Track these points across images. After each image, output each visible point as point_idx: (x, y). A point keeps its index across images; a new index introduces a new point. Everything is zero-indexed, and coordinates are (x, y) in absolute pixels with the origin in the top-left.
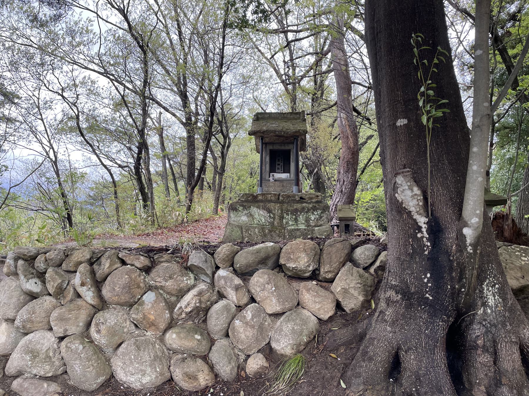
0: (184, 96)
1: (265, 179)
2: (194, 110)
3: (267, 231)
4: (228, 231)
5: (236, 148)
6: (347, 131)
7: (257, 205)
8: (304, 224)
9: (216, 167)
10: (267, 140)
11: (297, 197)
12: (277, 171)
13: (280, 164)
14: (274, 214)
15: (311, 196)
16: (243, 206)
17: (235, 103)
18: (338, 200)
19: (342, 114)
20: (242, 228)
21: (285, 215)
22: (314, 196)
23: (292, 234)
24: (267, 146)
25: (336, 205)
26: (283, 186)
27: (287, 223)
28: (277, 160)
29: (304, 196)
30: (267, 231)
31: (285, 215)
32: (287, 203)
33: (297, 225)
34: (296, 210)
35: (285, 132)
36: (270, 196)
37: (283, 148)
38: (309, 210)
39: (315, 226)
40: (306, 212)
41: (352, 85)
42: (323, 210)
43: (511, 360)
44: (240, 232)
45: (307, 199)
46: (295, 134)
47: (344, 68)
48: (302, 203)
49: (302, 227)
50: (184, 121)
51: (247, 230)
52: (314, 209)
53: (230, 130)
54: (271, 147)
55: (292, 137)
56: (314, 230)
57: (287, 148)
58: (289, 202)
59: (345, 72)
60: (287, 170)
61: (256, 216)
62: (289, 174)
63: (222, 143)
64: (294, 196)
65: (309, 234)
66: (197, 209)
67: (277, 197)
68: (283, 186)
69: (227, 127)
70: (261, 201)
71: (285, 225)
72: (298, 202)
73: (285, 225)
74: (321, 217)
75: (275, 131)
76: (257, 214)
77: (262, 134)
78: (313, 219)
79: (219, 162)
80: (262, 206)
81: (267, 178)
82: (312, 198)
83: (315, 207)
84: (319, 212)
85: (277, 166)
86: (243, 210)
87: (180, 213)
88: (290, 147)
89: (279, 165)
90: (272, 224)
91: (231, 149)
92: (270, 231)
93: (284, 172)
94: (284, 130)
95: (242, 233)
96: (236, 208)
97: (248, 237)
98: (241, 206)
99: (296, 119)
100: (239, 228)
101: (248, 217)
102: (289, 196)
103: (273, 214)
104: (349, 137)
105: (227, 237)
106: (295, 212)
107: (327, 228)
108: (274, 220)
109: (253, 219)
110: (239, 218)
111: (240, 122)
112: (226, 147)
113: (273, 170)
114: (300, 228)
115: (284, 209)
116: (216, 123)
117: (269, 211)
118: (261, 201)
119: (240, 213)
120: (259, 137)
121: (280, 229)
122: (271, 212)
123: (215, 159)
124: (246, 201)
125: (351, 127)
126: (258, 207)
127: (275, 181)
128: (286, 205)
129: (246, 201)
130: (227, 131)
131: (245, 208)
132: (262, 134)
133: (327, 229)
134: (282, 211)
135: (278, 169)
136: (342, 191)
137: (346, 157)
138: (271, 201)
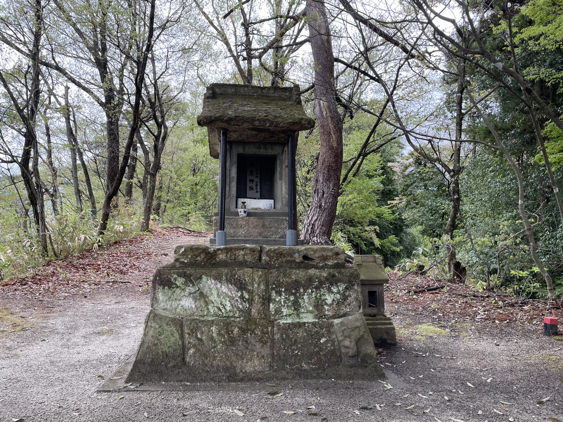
0: (102, 65)
1: (229, 209)
2: (118, 87)
3: (236, 330)
4: (151, 333)
5: (175, 140)
6: (328, 124)
7: (214, 272)
8: (311, 312)
9: (147, 164)
10: (233, 136)
11: (297, 255)
12: (249, 193)
13: (254, 181)
14: (250, 292)
15: (325, 254)
16: (184, 275)
17: (173, 84)
18: (315, 218)
19: (321, 102)
20: (181, 326)
21: (274, 294)
22: (330, 254)
23: (288, 336)
24: (234, 147)
25: (313, 225)
26: (264, 226)
27: (278, 311)
29: (310, 254)
30: (236, 330)
31: (274, 294)
32: (278, 268)
33: (298, 315)
34: (297, 284)
35: (271, 123)
36: (242, 252)
37: (263, 152)
38: (321, 283)
39: (334, 317)
40: (317, 288)
41: (335, 63)
42: (350, 282)
44: (177, 335)
45: (317, 261)
46: (291, 128)
47: (325, 38)
48: (307, 267)
49: (308, 318)
50: (104, 101)
51: (193, 332)
52: (332, 280)
53: (166, 117)
54: (241, 150)
55: (283, 132)
56: (332, 325)
57: (270, 152)
58: (280, 266)
59: (326, 44)
60: (267, 192)
61: (213, 297)
62: (272, 201)
63: (156, 134)
64: (291, 253)
65: (323, 336)
66: (116, 226)
67: (257, 255)
68: (264, 226)
69: (162, 112)
70: (225, 264)
71: (275, 315)
72: (299, 266)
73: (275, 315)
74: (345, 298)
75: (252, 120)
76: (215, 292)
77: (224, 125)
78: (329, 301)
79: (152, 159)
80: (226, 275)
82: (325, 258)
83: (334, 276)
84: (342, 287)
85: (249, 184)
86: (186, 284)
87: (89, 233)
88: (276, 150)
89: (252, 181)
90: (247, 313)
91: (168, 142)
92: (243, 331)
93: (262, 197)
94: (270, 117)
95: (182, 337)
96: (169, 280)
97: (194, 346)
98: (180, 276)
99: (284, 100)
100: (175, 325)
101: (195, 299)
102: (280, 254)
103: (249, 292)
104: (332, 133)
105: (149, 347)
106: (294, 288)
107: (357, 320)
108: (251, 304)
109: (207, 303)
110: (175, 304)
111: (181, 109)
112: (160, 140)
113: (242, 193)
114: (305, 320)
115: (271, 280)
116: (152, 109)
117: (241, 286)
118: (225, 264)
119: (178, 291)
120: (219, 129)
121: (263, 325)
122: (245, 289)
123: (146, 153)
124: (193, 264)
126: (218, 278)
127: (249, 214)
128: (275, 273)
129: (193, 264)
130: (163, 117)
131: (190, 279)
132: (224, 125)
133: (358, 324)
134: (267, 286)
135: (251, 188)
136: (320, 206)
137: (326, 160)
138: (243, 264)
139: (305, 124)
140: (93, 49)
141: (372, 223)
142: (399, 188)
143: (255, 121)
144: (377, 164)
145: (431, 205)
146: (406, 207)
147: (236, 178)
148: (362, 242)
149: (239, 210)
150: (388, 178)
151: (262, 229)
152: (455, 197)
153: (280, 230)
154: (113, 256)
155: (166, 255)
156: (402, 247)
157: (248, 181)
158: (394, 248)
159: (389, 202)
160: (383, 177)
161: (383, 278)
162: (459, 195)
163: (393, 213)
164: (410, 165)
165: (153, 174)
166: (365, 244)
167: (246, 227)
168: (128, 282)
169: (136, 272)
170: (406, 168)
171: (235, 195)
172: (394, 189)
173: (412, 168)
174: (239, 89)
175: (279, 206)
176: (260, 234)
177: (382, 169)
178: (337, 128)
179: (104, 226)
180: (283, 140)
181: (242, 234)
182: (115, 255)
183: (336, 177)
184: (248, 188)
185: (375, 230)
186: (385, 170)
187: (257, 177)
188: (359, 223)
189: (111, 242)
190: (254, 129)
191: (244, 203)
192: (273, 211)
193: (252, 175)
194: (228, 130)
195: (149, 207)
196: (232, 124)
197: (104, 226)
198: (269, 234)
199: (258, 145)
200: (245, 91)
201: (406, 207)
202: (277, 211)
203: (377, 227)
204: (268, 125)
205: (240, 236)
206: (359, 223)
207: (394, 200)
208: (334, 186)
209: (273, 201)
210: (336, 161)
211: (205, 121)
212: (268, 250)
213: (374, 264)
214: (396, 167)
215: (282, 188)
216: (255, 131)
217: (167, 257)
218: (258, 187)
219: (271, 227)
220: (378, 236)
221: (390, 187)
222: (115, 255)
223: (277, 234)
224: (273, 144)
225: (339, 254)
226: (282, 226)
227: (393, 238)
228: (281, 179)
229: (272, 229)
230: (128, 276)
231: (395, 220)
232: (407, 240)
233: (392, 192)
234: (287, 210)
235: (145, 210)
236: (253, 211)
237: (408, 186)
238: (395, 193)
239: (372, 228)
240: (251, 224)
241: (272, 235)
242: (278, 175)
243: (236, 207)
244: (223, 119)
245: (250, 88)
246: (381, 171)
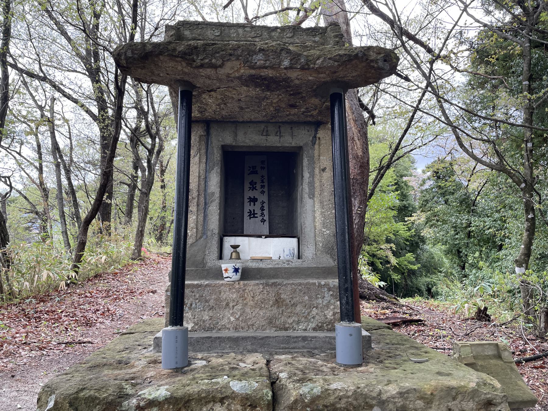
1: (203, 263)
10: (209, 104)
12: (249, 224)
26: (278, 302)
28: (247, 186)
43: (499, 409)
54: (228, 138)
60: (284, 225)
62: (293, 242)
66: (93, 258)
68: (278, 302)
81: (211, 259)
85: (248, 207)
89: (253, 200)
93: (271, 235)
125: (357, 123)
127: (246, 274)
135: (252, 215)
139: (376, 61)
140: (85, 60)
141: (388, 241)
142: (417, 204)
143: (256, 53)
144: (391, 180)
145: (455, 223)
146: (426, 223)
147: (217, 195)
148: (377, 261)
149: (224, 266)
150: (402, 193)
151: (275, 310)
152: (529, 217)
153: (315, 311)
154: (86, 297)
155: (154, 292)
156: (419, 265)
157: (246, 201)
158: (411, 266)
159: (406, 219)
160: (397, 193)
161: (526, 397)
162: (534, 214)
163: (409, 230)
164: (429, 179)
165: (146, 193)
166: (381, 263)
167: (239, 307)
168: (89, 342)
169: (107, 322)
170: (424, 182)
171: (216, 231)
172: (409, 204)
173: (432, 182)
174: (227, 31)
175: (309, 252)
176: (271, 322)
177: (396, 184)
178: (361, 133)
179: (78, 259)
180: (315, 113)
181: (230, 322)
182: (89, 295)
183: (362, 192)
184: (246, 215)
185: (391, 248)
186: (399, 185)
187: (263, 192)
188: (375, 241)
189: (90, 276)
190: (253, 81)
191: (235, 247)
192: (297, 263)
193: (254, 188)
194: (194, 87)
195: (141, 231)
196: (198, 62)
197: (78, 259)
198: (290, 321)
199: (263, 126)
200: (238, 34)
201: (426, 223)
202: (305, 265)
203: (392, 245)
204: (286, 63)
205: (224, 327)
206: (375, 241)
207: (411, 216)
208: (360, 204)
209: (295, 240)
210: (362, 172)
211: (129, 54)
212: (296, 401)
213: (500, 362)
214: (413, 182)
215: (316, 212)
216: (257, 85)
217: (156, 295)
218: (266, 212)
219: (295, 305)
220: (395, 254)
221: (404, 202)
222: (89, 295)
223: (309, 321)
224: (294, 124)
225: (495, 405)
226: (320, 301)
227: (410, 256)
228: (312, 196)
229: (298, 309)
230: (94, 329)
231: (411, 237)
232: (424, 257)
233: (407, 207)
234: (330, 262)
235: (137, 234)
236: (254, 265)
237: (427, 201)
238: (410, 209)
239: (388, 246)
240: (249, 298)
241: (298, 323)
242: (304, 187)
243: (221, 257)
244: (175, 50)
245: (248, 29)
246: (394, 187)
